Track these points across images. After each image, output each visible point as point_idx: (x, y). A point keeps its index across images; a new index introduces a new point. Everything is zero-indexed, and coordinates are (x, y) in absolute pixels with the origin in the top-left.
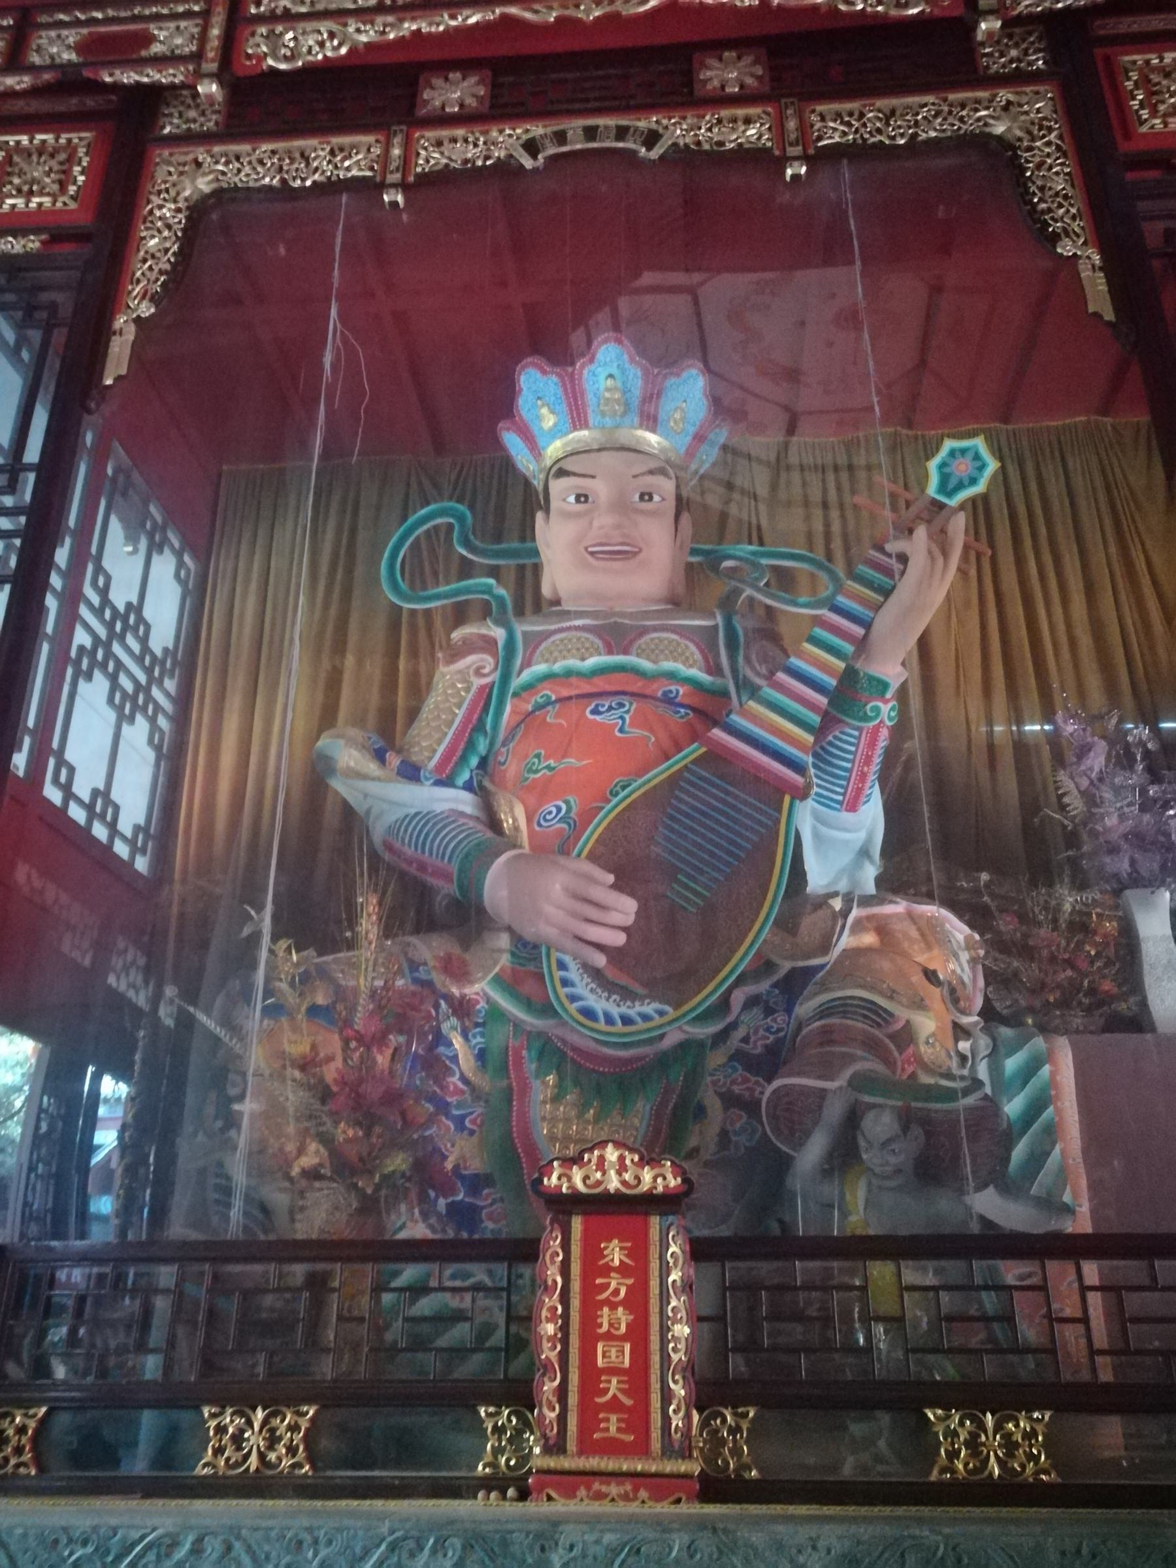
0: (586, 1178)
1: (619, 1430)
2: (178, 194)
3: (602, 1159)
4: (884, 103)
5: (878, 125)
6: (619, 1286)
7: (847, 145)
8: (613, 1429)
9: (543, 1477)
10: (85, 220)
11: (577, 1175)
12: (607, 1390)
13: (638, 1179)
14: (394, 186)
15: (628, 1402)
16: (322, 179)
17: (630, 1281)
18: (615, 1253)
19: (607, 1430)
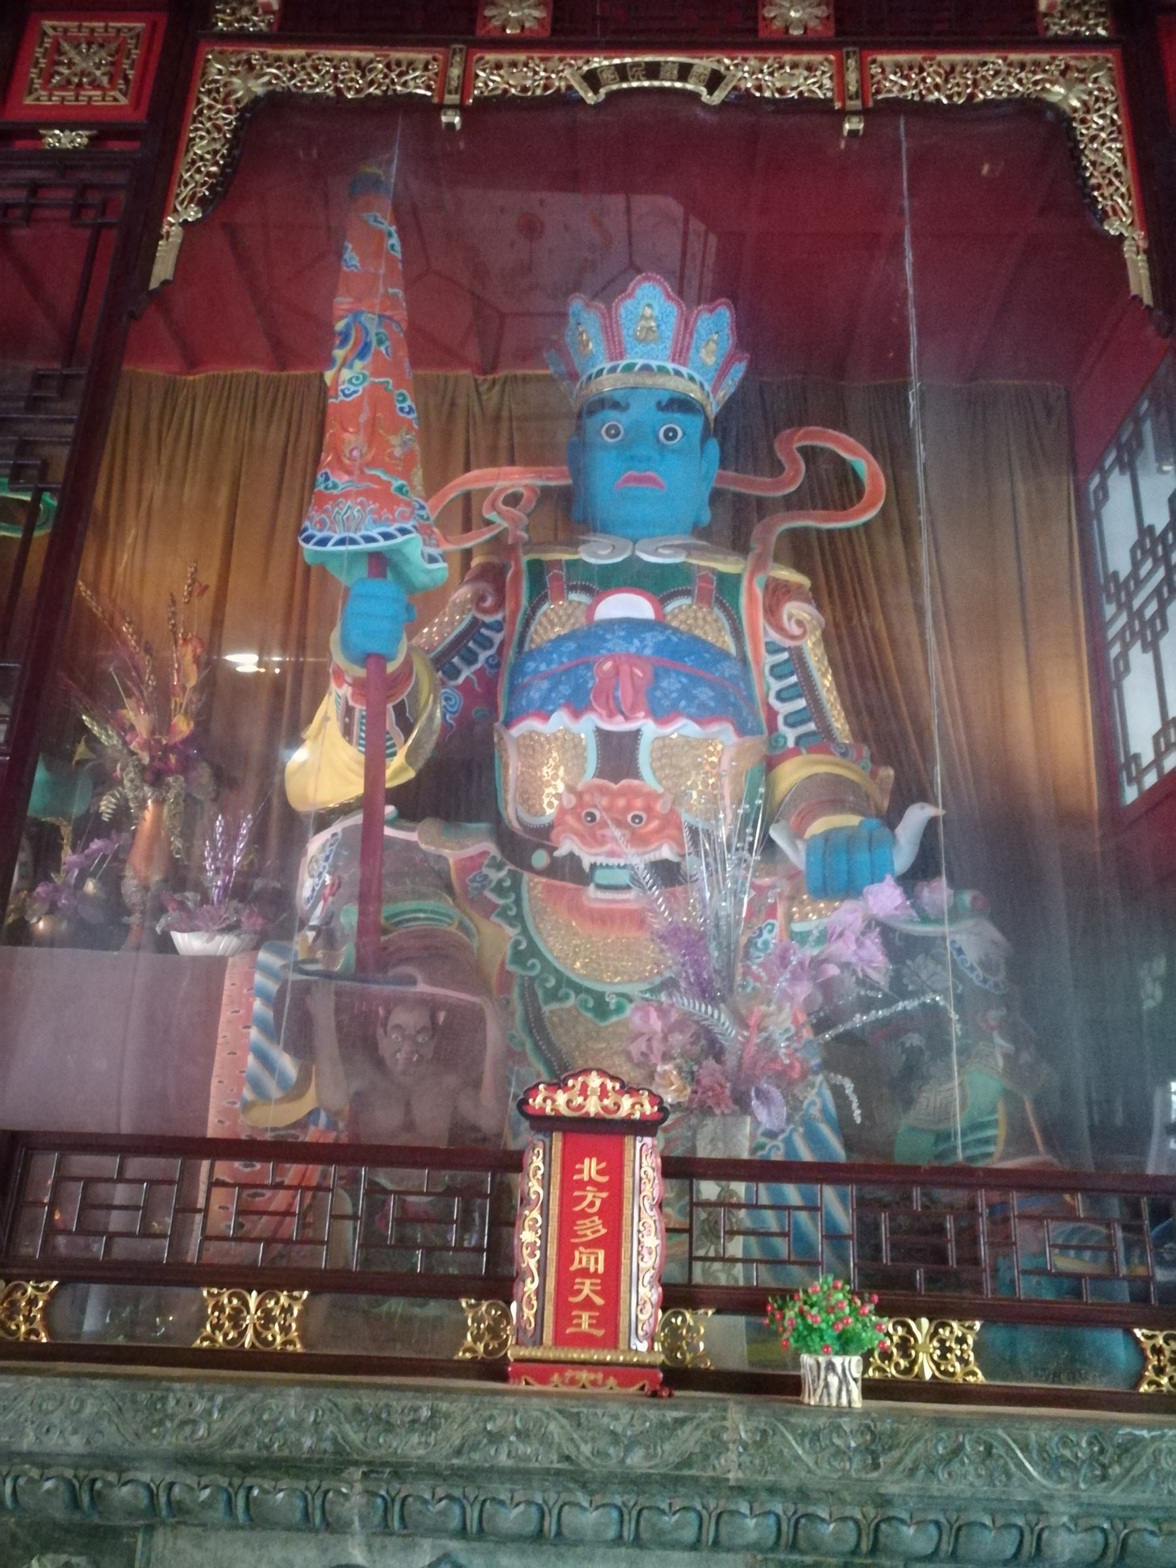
0: (569, 1102)
1: (590, 1325)
2: (228, 95)
3: (585, 1086)
4: (946, 58)
5: (938, 80)
6: (593, 1198)
7: (904, 101)
8: (585, 1326)
9: (518, 1365)
10: (139, 117)
11: (561, 1098)
12: (580, 1291)
13: (618, 1106)
14: (452, 107)
15: (599, 1301)
16: (378, 92)
17: (604, 1195)
18: (590, 1168)
19: (580, 1325)
